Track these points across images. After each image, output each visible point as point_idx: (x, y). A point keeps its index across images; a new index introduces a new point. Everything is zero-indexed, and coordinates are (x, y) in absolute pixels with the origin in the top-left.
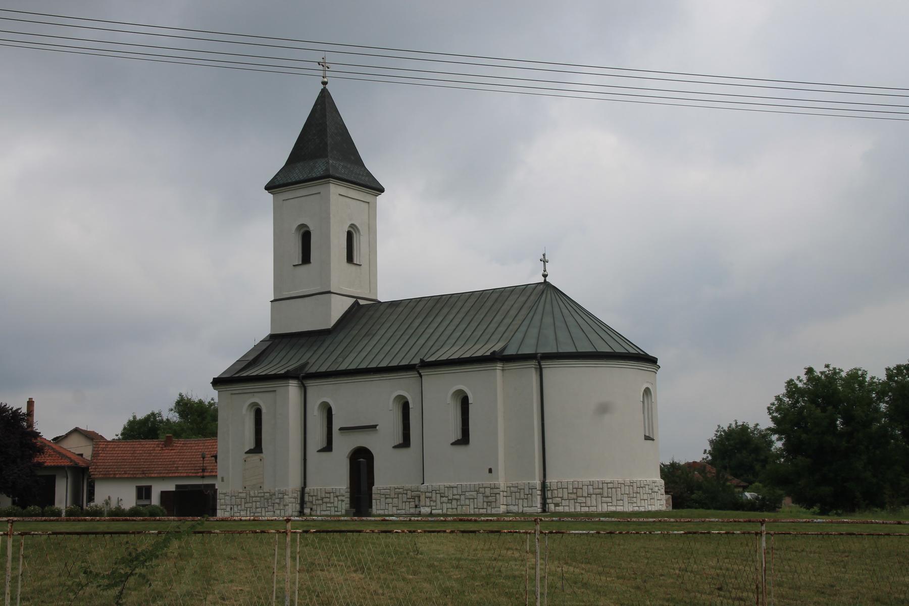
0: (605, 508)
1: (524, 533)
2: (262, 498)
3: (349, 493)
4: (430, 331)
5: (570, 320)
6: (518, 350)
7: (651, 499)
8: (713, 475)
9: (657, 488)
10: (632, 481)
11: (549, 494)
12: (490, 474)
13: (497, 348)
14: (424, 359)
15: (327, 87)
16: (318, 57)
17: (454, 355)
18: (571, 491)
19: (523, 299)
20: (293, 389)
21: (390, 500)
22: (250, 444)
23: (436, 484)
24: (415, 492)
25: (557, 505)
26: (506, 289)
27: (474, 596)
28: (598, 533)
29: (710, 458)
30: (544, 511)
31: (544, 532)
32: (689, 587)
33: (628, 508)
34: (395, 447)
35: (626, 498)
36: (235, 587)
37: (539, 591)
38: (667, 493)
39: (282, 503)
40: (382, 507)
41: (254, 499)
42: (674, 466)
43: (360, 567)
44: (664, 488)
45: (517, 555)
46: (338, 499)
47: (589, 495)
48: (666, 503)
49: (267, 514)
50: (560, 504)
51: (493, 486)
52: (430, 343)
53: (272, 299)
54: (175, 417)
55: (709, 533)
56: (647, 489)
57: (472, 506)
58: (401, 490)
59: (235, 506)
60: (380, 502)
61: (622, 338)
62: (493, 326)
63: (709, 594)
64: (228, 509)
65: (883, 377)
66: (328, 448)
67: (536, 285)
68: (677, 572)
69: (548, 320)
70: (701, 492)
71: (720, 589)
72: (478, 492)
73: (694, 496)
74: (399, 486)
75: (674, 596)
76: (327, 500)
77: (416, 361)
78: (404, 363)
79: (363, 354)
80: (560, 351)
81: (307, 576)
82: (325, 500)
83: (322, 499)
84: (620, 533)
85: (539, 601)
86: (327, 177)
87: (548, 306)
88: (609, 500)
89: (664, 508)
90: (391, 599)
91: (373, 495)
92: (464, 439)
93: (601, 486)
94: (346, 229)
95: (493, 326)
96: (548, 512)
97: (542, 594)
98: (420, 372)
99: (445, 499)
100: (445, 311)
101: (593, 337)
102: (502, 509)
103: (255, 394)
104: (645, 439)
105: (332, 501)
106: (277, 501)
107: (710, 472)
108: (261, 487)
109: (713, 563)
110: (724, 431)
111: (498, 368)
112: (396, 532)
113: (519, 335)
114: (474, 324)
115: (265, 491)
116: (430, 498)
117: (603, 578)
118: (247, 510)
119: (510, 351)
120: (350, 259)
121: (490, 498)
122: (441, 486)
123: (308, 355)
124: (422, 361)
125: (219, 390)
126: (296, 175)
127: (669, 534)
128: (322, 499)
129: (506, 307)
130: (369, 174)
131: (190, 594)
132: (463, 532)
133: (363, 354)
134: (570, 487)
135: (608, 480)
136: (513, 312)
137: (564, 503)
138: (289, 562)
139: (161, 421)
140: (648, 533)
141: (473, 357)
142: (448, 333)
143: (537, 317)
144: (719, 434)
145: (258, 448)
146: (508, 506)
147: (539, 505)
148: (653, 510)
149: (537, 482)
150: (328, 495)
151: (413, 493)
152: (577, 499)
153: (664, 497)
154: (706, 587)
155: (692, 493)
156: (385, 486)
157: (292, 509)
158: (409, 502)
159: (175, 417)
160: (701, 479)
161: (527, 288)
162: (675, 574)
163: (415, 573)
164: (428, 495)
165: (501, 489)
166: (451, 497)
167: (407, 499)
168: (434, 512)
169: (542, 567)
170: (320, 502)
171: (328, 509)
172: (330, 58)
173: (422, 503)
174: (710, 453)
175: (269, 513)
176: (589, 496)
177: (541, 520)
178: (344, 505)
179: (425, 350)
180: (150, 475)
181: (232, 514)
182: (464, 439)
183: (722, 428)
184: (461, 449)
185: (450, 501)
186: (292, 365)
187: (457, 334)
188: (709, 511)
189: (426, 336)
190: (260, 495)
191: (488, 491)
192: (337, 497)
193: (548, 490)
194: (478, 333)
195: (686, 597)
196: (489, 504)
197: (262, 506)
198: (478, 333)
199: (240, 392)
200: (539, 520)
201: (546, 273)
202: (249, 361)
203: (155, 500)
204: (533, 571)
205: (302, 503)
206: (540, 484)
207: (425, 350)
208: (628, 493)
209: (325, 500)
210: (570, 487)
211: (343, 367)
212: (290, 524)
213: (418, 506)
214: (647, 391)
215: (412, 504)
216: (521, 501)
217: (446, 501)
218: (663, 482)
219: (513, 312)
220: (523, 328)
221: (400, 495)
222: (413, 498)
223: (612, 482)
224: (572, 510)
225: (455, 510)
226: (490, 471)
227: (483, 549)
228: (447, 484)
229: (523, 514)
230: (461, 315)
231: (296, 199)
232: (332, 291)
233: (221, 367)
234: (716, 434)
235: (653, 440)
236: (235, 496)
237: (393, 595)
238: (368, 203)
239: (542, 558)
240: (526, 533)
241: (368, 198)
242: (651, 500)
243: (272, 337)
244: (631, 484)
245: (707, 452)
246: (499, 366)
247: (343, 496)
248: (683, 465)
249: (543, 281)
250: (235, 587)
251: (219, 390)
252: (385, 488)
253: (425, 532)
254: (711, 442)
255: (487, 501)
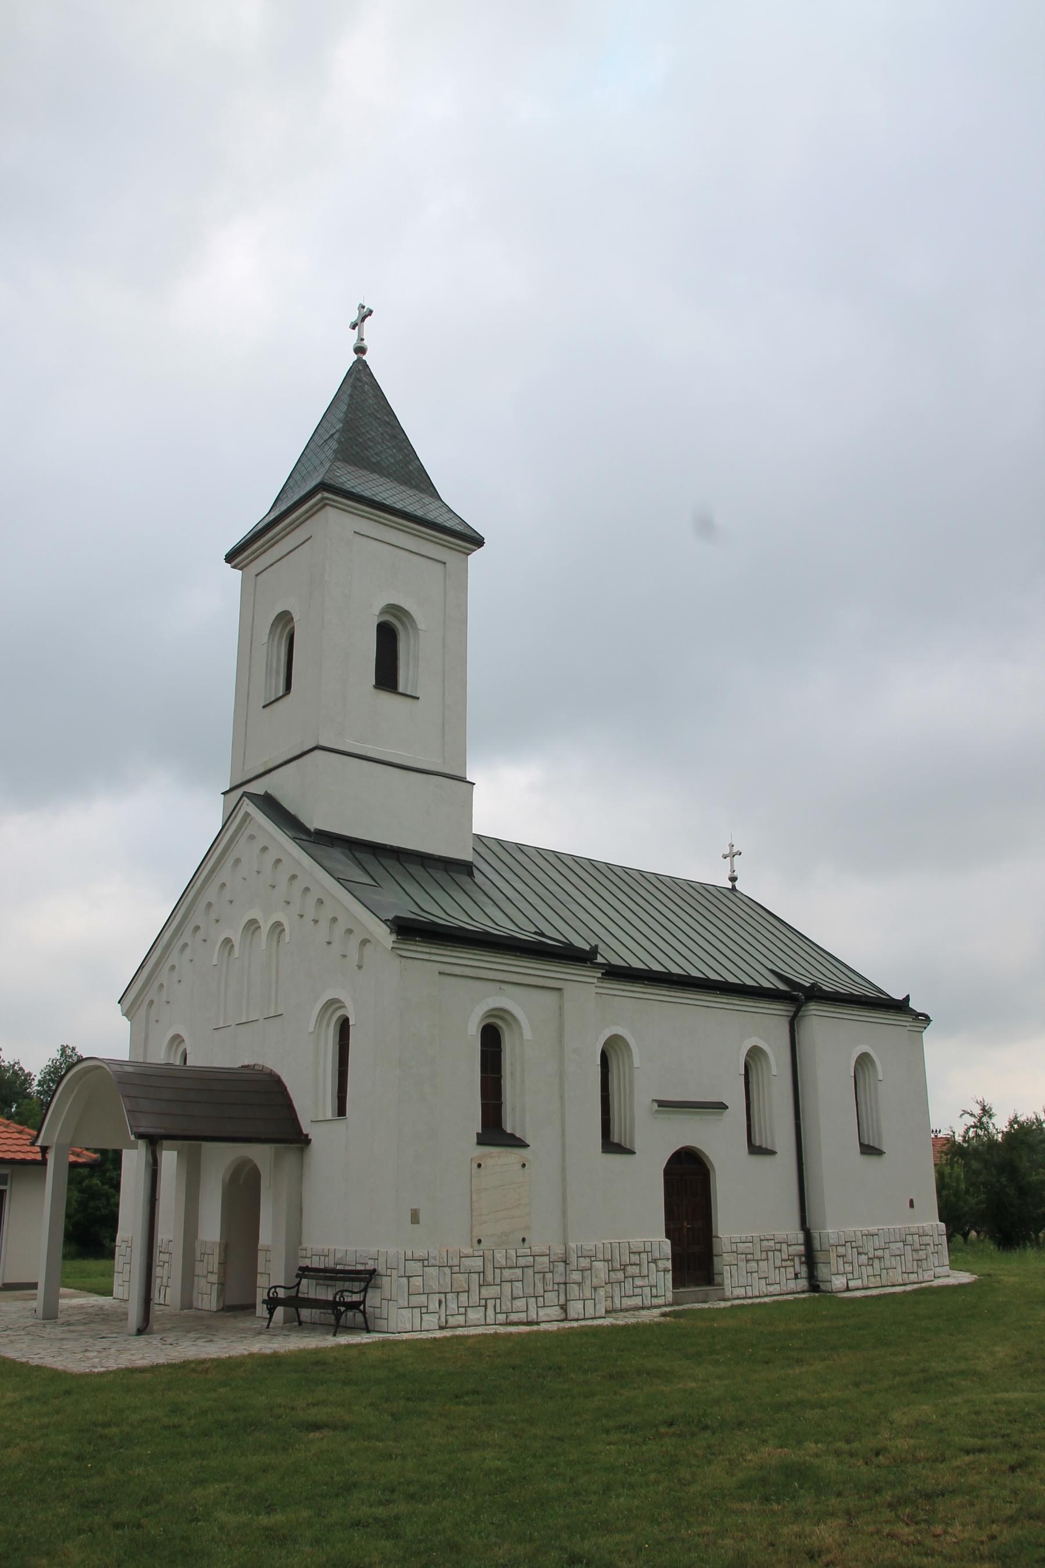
2: (530, 1271)
12: (912, 1209)
21: (754, 1264)
39: (588, 1282)
40: (743, 1281)
41: (507, 1273)
46: (657, 1266)
49: (541, 1312)
58: (772, 1243)
59: (449, 1296)
64: (434, 1306)
65: (981, 1112)
76: (634, 1270)
82: (632, 1270)
83: (624, 1268)
91: (320, 1267)
99: (863, 1258)
103: (503, 986)
105: (645, 1272)
106: (576, 1276)
108: (524, 1240)
115: (536, 1250)
116: (843, 1256)
118: (486, 1306)
128: (624, 1268)
150: (635, 1258)
158: (786, 1267)
164: (841, 1250)
167: (782, 1260)
168: (852, 1284)
170: (620, 1275)
171: (638, 1291)
175: (548, 1310)
181: (443, 1319)
190: (522, 1262)
192: (655, 1261)
196: (920, 1263)
197: (530, 1291)
199: (426, 957)
209: (632, 1270)
221: (770, 1254)
225: (878, 1278)
228: (865, 1229)
236: (451, 1267)
238: (445, 563)
252: (744, 1239)
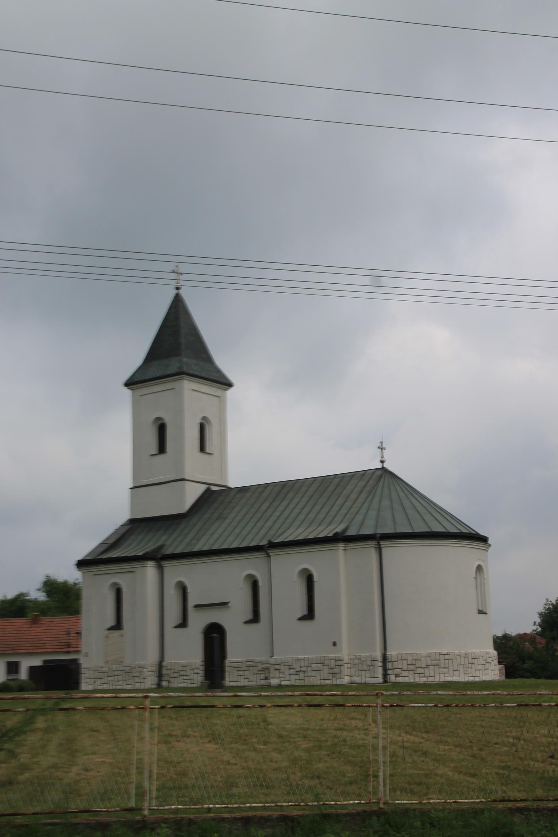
0: (443, 678)
1: (366, 706)
3: (204, 672)
4: (277, 514)
5: (406, 503)
6: (360, 530)
7: (485, 669)
8: (543, 645)
9: (490, 659)
10: (467, 653)
11: (389, 666)
12: (335, 647)
13: (339, 529)
14: (272, 540)
15: (181, 292)
16: (172, 266)
17: (298, 537)
18: (410, 663)
19: (362, 483)
20: (150, 569)
22: (111, 621)
23: (284, 657)
24: (265, 665)
25: (397, 676)
26: (347, 474)
27: (320, 765)
28: (436, 706)
29: (539, 629)
30: (385, 681)
31: (385, 705)
32: (522, 755)
33: (464, 678)
34: (246, 622)
35: (461, 669)
36: (98, 759)
37: (381, 759)
38: (500, 663)
42: (506, 637)
43: (214, 738)
44: (497, 659)
45: (360, 724)
47: (427, 666)
48: (500, 673)
50: (401, 675)
51: (337, 658)
52: (277, 525)
53: (132, 486)
54: (41, 597)
55: (540, 705)
56: (481, 660)
57: (318, 678)
60: (233, 674)
61: (455, 518)
62: (336, 508)
63: (542, 762)
66: (183, 624)
67: (375, 470)
68: (511, 740)
69: (386, 503)
70: (531, 662)
71: (552, 757)
72: (323, 664)
73: (525, 666)
74: (250, 659)
75: (509, 764)
77: (264, 542)
78: (253, 544)
79: (215, 536)
80: (398, 531)
81: (164, 747)
84: (456, 706)
85: (381, 770)
86: (180, 374)
87: (386, 490)
88: (445, 670)
89: (497, 678)
90: (243, 768)
92: (310, 615)
93: (438, 658)
94: (198, 421)
95: (336, 508)
96: (390, 682)
97: (384, 763)
98: (269, 552)
99: (292, 671)
100: (291, 495)
101: (428, 518)
102: (346, 680)
104: (479, 613)
107: (540, 643)
109: (545, 731)
110: (552, 604)
111: (340, 548)
112: (248, 707)
113: (359, 517)
114: (317, 508)
115: (126, 665)
117: (441, 747)
119: (352, 532)
120: (202, 448)
121: (335, 670)
122: (289, 659)
123: (164, 537)
124: (270, 542)
125: (84, 571)
126: (153, 372)
127: (503, 706)
129: (346, 491)
130: (218, 371)
131: (54, 766)
132: (310, 706)
133: (215, 536)
134: (409, 658)
135: (445, 652)
136: (353, 496)
137: (404, 674)
138: (147, 735)
139: (29, 601)
140: (482, 705)
141: (317, 538)
142: (293, 515)
143: (376, 500)
144: (547, 607)
145: (118, 626)
146: (352, 677)
147: (380, 676)
148: (488, 679)
149: (378, 655)
151: (263, 665)
152: (416, 670)
153: (498, 667)
154: (539, 755)
155: (524, 663)
156: (238, 659)
157: (150, 682)
159: (41, 597)
160: (531, 649)
161: (366, 474)
162: (509, 742)
163: (265, 743)
164: (277, 667)
165: (345, 661)
166: (298, 669)
169: (384, 736)
172: (183, 268)
173: (271, 675)
174: (540, 626)
176: (427, 667)
177: (382, 694)
178: (198, 678)
179: (272, 533)
180: (18, 651)
182: (310, 615)
183: (550, 601)
184: (307, 624)
185: (297, 673)
186: (150, 547)
187: (302, 517)
188: (540, 681)
189: (273, 519)
191: (332, 662)
193: (389, 662)
194: (321, 516)
195: (520, 765)
198: (321, 516)
200: (380, 694)
201: (383, 459)
202: (111, 544)
203: (23, 675)
204: (375, 740)
205: (160, 676)
206: (381, 656)
207: (272, 533)
208: (464, 664)
210: (409, 658)
211: (197, 548)
212: (149, 700)
213: (268, 678)
214: (479, 568)
215: (262, 676)
216: (363, 673)
217: (295, 673)
218: (495, 653)
219: (353, 496)
220: (363, 511)
222: (263, 670)
223: (449, 653)
224: (412, 680)
226: (335, 644)
227: (329, 720)
228: (295, 657)
229: (365, 684)
230: (305, 499)
231: (153, 394)
232: (187, 478)
233: (83, 552)
234: (545, 607)
235: (485, 613)
237: (245, 765)
239: (384, 728)
240: (369, 706)
241: (218, 392)
242: (486, 670)
243: (132, 521)
244: (466, 656)
245: (537, 624)
246: (341, 546)
247: (199, 669)
248: (515, 636)
249: (381, 467)
250: (98, 759)
251: (84, 571)
253: (275, 706)
254: (541, 614)
255: (332, 672)
